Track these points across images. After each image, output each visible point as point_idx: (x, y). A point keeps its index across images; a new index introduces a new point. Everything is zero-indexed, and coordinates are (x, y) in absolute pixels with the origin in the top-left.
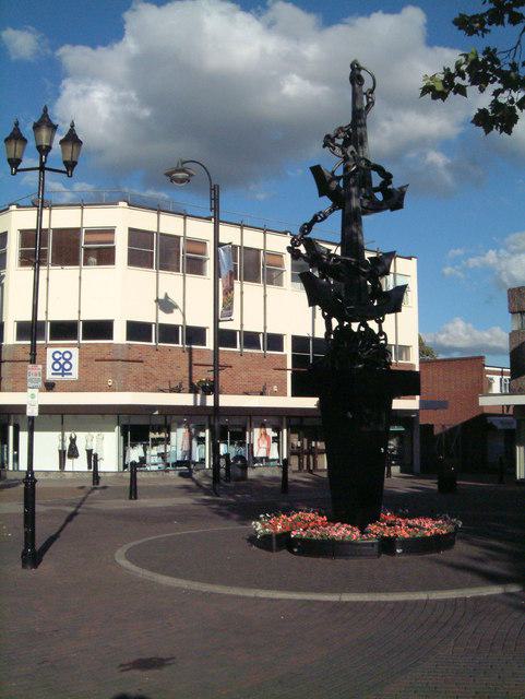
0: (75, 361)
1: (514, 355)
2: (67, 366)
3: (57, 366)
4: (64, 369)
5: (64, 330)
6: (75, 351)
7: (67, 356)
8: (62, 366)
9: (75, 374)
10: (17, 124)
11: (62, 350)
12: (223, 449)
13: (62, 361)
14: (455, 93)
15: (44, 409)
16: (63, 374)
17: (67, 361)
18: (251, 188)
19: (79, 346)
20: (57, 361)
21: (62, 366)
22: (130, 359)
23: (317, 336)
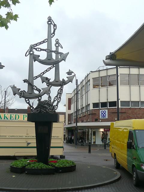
0: (107, 113)
1: (10, 171)
2: (105, 115)
3: (102, 115)
4: (104, 116)
5: (104, 105)
6: (107, 111)
7: (105, 112)
8: (103, 115)
9: (107, 117)
10: (68, 53)
11: (103, 110)
12: (102, 130)
13: (103, 114)
14: (14, 20)
15: (78, 117)
16: (104, 117)
17: (105, 113)
18: (107, 189)
19: (108, 109)
20: (102, 113)
21: (103, 115)
22: (123, 112)
23: (51, 149)
